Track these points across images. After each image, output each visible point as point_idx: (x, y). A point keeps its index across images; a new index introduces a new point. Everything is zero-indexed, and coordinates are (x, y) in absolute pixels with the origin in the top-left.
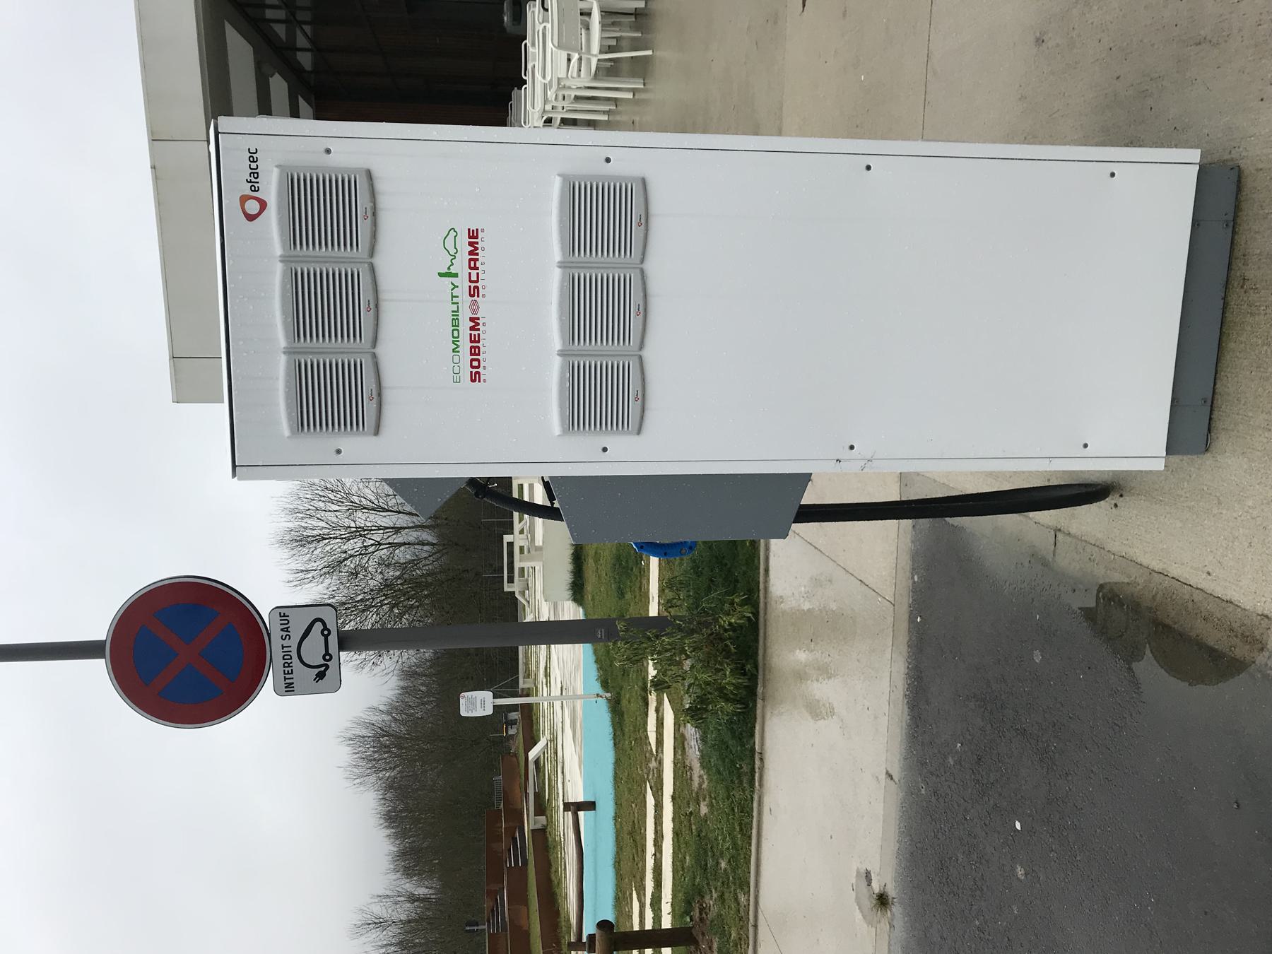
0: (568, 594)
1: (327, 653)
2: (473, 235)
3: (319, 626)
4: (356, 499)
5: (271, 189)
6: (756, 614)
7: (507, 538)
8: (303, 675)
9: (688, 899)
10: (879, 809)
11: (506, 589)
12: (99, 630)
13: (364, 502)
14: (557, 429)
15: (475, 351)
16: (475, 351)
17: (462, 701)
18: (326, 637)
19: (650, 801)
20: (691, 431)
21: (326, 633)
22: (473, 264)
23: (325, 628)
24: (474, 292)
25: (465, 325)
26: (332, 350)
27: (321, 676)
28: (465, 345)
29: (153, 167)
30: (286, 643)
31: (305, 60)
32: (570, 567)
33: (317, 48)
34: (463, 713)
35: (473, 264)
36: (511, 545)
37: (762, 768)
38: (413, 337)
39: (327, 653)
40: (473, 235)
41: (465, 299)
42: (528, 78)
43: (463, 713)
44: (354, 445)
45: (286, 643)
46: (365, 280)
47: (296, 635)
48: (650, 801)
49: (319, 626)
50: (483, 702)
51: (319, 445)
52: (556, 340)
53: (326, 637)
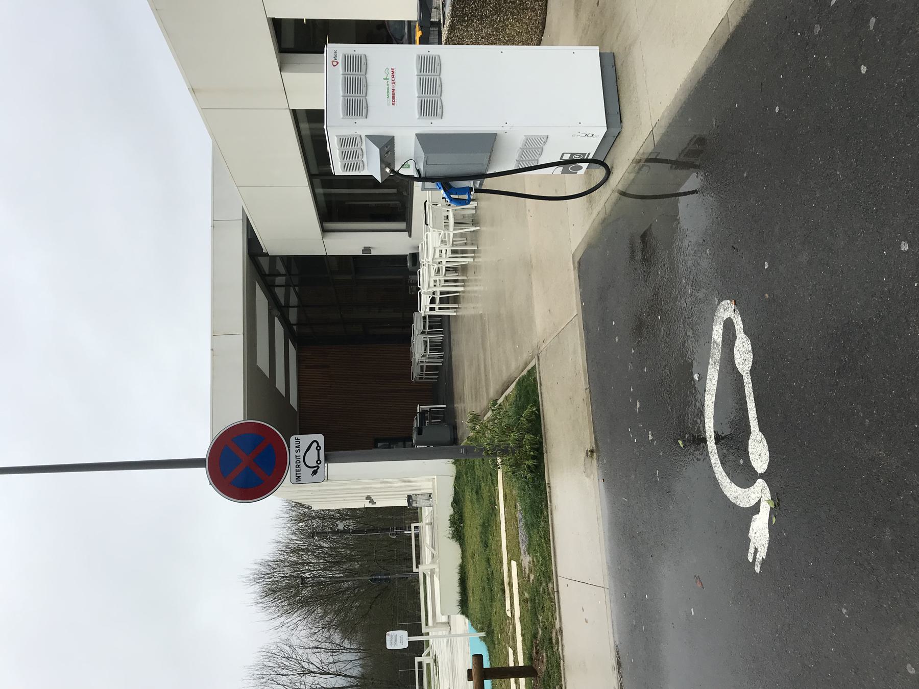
0: (458, 609)
1: (319, 459)
2: (393, 69)
3: (315, 445)
4: (306, 665)
5: (340, 59)
6: (538, 410)
7: (418, 659)
8: (306, 472)
9: (529, 657)
10: (586, 414)
11: (415, 570)
12: (202, 453)
13: (312, 668)
14: (417, 116)
15: (393, 98)
16: (393, 98)
17: (388, 638)
18: (318, 451)
19: (511, 651)
20: (453, 121)
21: (318, 448)
22: (393, 76)
23: (318, 446)
24: (393, 83)
25: (391, 91)
26: (355, 96)
27: (315, 472)
28: (391, 96)
29: (212, 350)
30: (298, 454)
31: (293, 316)
32: (458, 589)
33: (301, 306)
34: (389, 647)
35: (393, 76)
36: (420, 664)
37: (550, 493)
38: (376, 94)
39: (319, 459)
40: (393, 69)
41: (391, 85)
42: (421, 287)
43: (389, 647)
44: (360, 121)
45: (298, 454)
46: (364, 80)
47: (303, 448)
48: (511, 651)
49: (315, 445)
50: (401, 638)
51: (350, 121)
52: (415, 72)
53: (318, 451)
